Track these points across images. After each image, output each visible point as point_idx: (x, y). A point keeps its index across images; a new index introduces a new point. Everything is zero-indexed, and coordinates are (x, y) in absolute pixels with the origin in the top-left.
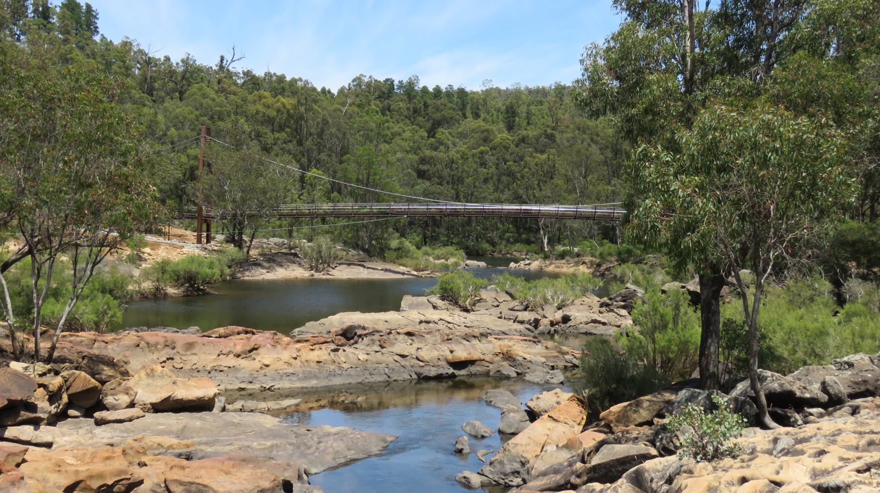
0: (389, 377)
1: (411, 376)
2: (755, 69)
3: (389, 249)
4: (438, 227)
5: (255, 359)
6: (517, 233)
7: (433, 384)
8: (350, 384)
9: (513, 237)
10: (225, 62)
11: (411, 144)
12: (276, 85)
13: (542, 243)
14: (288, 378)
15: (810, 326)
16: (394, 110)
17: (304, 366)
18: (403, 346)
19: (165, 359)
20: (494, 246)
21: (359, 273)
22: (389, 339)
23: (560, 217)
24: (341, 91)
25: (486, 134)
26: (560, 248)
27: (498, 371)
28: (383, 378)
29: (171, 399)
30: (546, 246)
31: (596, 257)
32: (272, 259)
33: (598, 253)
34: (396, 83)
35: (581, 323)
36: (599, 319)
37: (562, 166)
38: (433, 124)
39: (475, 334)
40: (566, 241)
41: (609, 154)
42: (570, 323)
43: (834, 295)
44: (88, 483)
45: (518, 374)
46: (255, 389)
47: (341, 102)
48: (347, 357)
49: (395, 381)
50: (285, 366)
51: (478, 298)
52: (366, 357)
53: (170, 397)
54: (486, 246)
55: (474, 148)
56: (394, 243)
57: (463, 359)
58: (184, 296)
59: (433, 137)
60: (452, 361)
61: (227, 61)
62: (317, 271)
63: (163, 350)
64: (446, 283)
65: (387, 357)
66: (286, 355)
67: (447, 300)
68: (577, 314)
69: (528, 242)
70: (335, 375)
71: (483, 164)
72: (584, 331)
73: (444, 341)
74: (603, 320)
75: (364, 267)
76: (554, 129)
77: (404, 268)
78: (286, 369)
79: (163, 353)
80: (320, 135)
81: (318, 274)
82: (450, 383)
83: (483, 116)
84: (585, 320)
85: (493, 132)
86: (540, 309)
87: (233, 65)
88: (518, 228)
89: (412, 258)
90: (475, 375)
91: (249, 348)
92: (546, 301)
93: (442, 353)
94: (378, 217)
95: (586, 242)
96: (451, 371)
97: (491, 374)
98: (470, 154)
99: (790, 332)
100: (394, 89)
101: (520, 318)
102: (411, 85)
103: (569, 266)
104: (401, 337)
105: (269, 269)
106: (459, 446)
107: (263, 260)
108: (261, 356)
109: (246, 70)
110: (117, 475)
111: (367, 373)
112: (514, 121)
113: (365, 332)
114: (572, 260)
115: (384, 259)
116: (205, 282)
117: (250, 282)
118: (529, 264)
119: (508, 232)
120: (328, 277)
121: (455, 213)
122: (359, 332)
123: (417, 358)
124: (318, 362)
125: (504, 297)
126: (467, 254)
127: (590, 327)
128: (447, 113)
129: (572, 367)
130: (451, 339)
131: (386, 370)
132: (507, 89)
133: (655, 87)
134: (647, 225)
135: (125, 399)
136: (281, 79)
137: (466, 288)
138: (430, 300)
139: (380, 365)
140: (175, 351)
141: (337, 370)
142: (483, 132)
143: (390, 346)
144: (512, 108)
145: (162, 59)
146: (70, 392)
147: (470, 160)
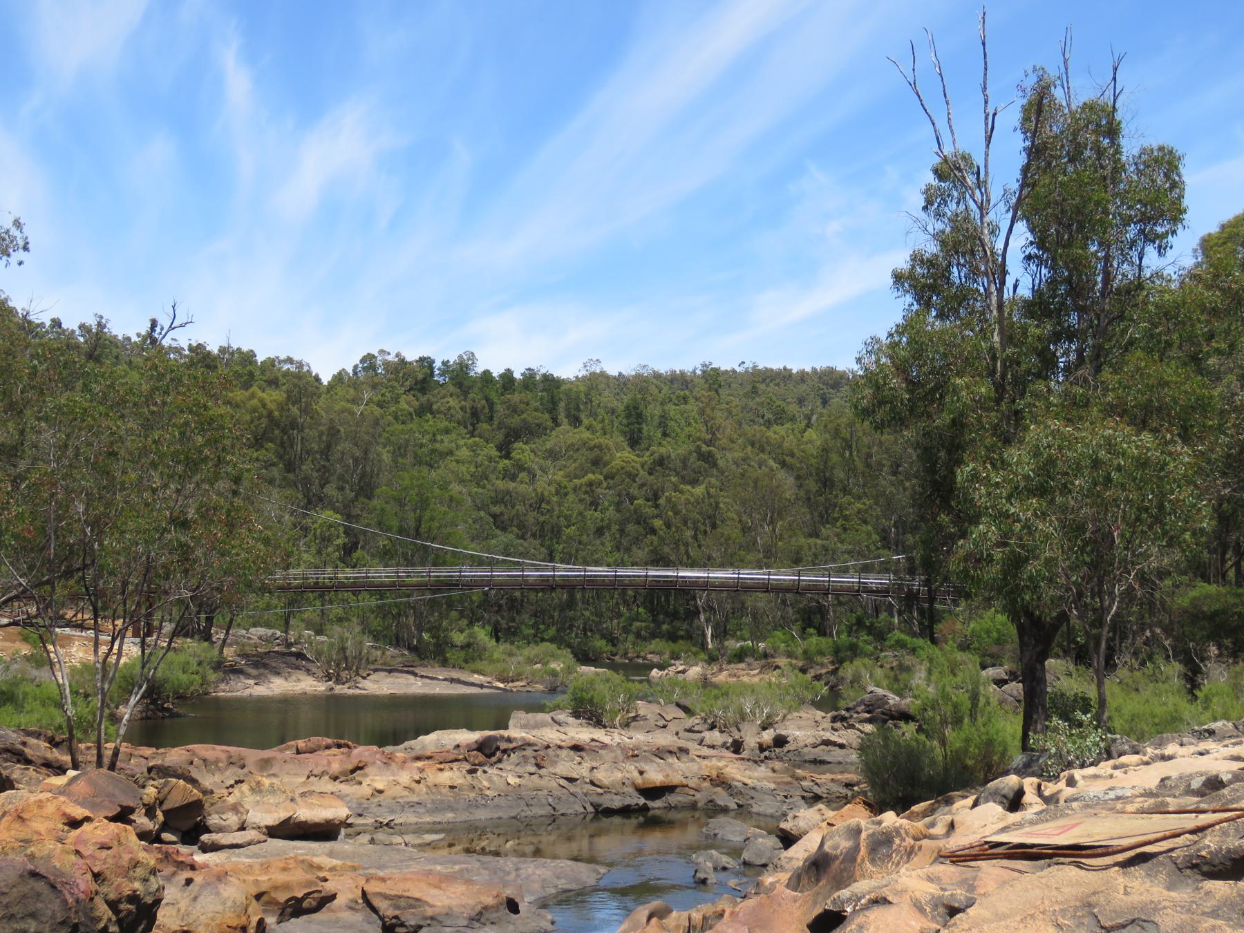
0: (554, 809)
1: (585, 808)
2: (1081, 372)
3: (453, 646)
4: (518, 613)
5: (360, 783)
6: (654, 621)
7: (617, 820)
8: (500, 818)
9: (647, 628)
10: (158, 329)
11: (472, 469)
12: (238, 368)
13: (704, 635)
14: (413, 809)
15: (1159, 710)
16: (439, 412)
17: (432, 793)
18: (567, 765)
19: (232, 782)
20: (614, 645)
21: (408, 685)
22: (548, 755)
23: (738, 589)
24: (339, 378)
25: (597, 452)
26: (733, 645)
27: (711, 801)
28: (547, 810)
29: (292, 822)
30: (709, 640)
31: (796, 658)
32: (261, 663)
33: (799, 651)
34: (438, 364)
35: (806, 746)
36: (833, 738)
37: (729, 506)
38: (507, 436)
39: (671, 749)
41: (813, 485)
42: (787, 747)
43: (1187, 681)
44: (273, 895)
45: (740, 806)
46: (367, 825)
47: (350, 398)
48: (490, 780)
49: (563, 815)
50: (406, 793)
51: (633, 715)
52: (518, 780)
53: (290, 818)
54: (600, 644)
55: (576, 477)
56: (459, 638)
57: (658, 784)
58: (142, 719)
59: (508, 456)
60: (642, 787)
61: (162, 329)
62: (338, 681)
63: (226, 769)
64: (582, 690)
65: (548, 782)
66: (405, 778)
67: (584, 718)
68: (798, 733)
69: (673, 637)
70: (477, 807)
71: (595, 504)
72: (811, 757)
73: (628, 758)
74: (840, 741)
75: (415, 675)
76: (709, 443)
77: (481, 677)
78: (407, 796)
79: (228, 773)
80: (326, 452)
81: (340, 686)
82: (641, 819)
83: (586, 422)
84: (810, 741)
85: (609, 449)
86: (734, 730)
87: (172, 334)
88: (652, 611)
89: (492, 661)
90: (676, 807)
91: (350, 767)
92: (743, 717)
93: (627, 775)
94: (434, 592)
95: (778, 634)
96: (642, 801)
97: (700, 805)
98: (570, 486)
99: (1132, 720)
100: (432, 374)
101: (708, 741)
103: (752, 673)
104: (564, 753)
105: (259, 679)
106: (701, 875)
107: (245, 664)
108: (370, 777)
109: (195, 344)
110: (306, 887)
111: (522, 803)
112: (640, 431)
113: (511, 746)
114: (756, 664)
115: (444, 663)
116: (181, 697)
117: (228, 701)
118: (684, 672)
119: (637, 619)
120: (358, 692)
121: (549, 586)
122: (503, 745)
123: (592, 783)
124: (452, 787)
125: (673, 712)
126: (575, 655)
127: (821, 752)
129: (812, 798)
130: (637, 756)
131: (550, 800)
132: (620, 374)
133: (964, 393)
134: (982, 553)
135: (232, 819)
136: (249, 358)
137: (613, 698)
138: (555, 718)
139: (539, 793)
140: (245, 770)
141: (479, 799)
142: (591, 449)
143: (552, 765)
144: (636, 408)
145: (48, 323)
146: (165, 807)
147: (571, 497)
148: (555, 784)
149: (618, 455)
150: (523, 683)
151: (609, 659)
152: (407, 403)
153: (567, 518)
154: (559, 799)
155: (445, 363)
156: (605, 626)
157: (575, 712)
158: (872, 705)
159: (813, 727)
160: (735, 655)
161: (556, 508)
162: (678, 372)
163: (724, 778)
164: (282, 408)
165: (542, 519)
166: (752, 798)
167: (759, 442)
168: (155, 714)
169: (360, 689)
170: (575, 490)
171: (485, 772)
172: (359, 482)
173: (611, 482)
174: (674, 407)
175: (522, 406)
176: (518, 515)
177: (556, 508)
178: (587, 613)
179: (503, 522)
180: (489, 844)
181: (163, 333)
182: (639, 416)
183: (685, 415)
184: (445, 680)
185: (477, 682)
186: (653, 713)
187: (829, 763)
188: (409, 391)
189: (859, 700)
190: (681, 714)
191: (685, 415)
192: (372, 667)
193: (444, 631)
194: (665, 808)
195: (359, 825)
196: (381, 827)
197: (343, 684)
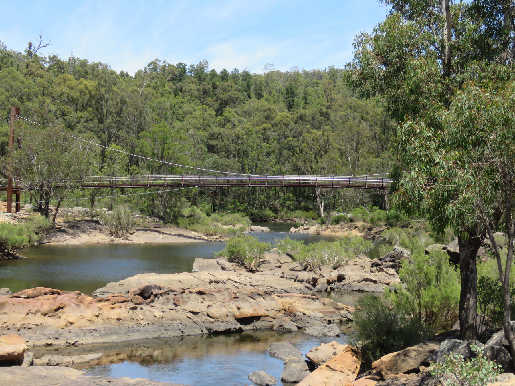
0: (182, 332)
1: (202, 331)
3: (182, 216)
4: (226, 196)
5: (60, 317)
6: (297, 201)
7: (222, 338)
8: (147, 338)
10: (33, 48)
11: (202, 122)
14: (91, 334)
17: (106, 323)
20: (276, 213)
22: (182, 297)
24: (138, 74)
25: (268, 112)
27: (281, 326)
28: (178, 333)
30: (322, 212)
31: (367, 222)
33: (368, 219)
34: (188, 67)
35: (355, 281)
36: (370, 277)
38: (221, 104)
40: (341, 208)
41: (378, 130)
42: (344, 282)
45: (299, 328)
46: (61, 345)
48: (144, 314)
49: (188, 335)
50: (88, 323)
52: (161, 314)
54: (269, 213)
55: (257, 125)
57: (249, 315)
59: (221, 115)
60: (239, 317)
61: (35, 48)
62: (117, 236)
64: (233, 247)
66: (89, 314)
67: (235, 262)
68: (351, 274)
69: (307, 209)
70: (133, 331)
71: (266, 140)
72: (357, 288)
73: (231, 299)
74: (374, 279)
75: (159, 232)
78: (89, 326)
80: (119, 113)
82: (238, 337)
83: (265, 96)
84: (358, 278)
85: (274, 111)
86: (317, 270)
87: (40, 51)
88: (297, 196)
89: (203, 224)
90: (260, 329)
91: (55, 307)
92: (323, 262)
93: (230, 310)
94: (172, 188)
96: (238, 326)
97: (274, 328)
101: (300, 278)
102: (201, 68)
104: (193, 296)
105: (73, 236)
107: (67, 227)
109: (52, 56)
111: (162, 328)
112: (293, 101)
114: (346, 225)
115: (177, 225)
118: (308, 229)
120: (127, 242)
121: (241, 184)
122: (155, 291)
123: (208, 315)
124: (118, 319)
128: (233, 94)
129: (347, 321)
130: (238, 297)
131: (180, 326)
132: (287, 72)
139: (174, 322)
141: (135, 326)
142: (265, 111)
143: (183, 304)
148: (185, 316)
149: (280, 114)
150: (218, 237)
151: (273, 220)
152: (169, 87)
153: (252, 147)
154: (186, 325)
155: (192, 66)
156: (271, 203)
157: (230, 259)
158: (394, 257)
159: (360, 270)
160: (335, 220)
161: (246, 142)
162: (317, 71)
163: (292, 310)
164: (97, 89)
165: (238, 148)
166: (308, 323)
167: (354, 106)
168: (3, 257)
169: (129, 240)
170: (257, 132)
171: (142, 309)
172: (138, 128)
173: (275, 128)
174: (312, 88)
175: (229, 88)
176: (225, 146)
177: (246, 142)
178: (262, 197)
179: (217, 149)
180: (144, 352)
181: (35, 50)
182: (293, 93)
183: (317, 93)
184: (175, 235)
185: (192, 236)
186: (274, 259)
187: (367, 291)
188: (170, 80)
189: (387, 254)
190: (289, 260)
191: (317, 93)
192: (137, 228)
193: (178, 208)
194: (253, 329)
195: (55, 345)
196: (69, 346)
197: (120, 238)
